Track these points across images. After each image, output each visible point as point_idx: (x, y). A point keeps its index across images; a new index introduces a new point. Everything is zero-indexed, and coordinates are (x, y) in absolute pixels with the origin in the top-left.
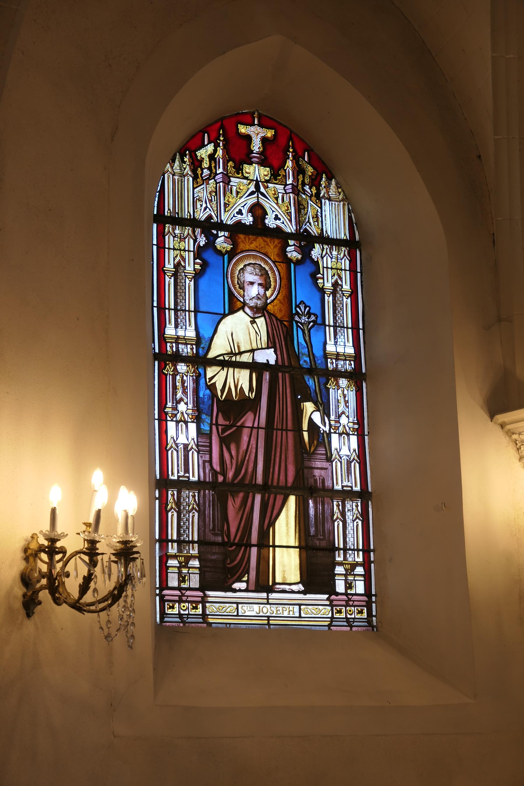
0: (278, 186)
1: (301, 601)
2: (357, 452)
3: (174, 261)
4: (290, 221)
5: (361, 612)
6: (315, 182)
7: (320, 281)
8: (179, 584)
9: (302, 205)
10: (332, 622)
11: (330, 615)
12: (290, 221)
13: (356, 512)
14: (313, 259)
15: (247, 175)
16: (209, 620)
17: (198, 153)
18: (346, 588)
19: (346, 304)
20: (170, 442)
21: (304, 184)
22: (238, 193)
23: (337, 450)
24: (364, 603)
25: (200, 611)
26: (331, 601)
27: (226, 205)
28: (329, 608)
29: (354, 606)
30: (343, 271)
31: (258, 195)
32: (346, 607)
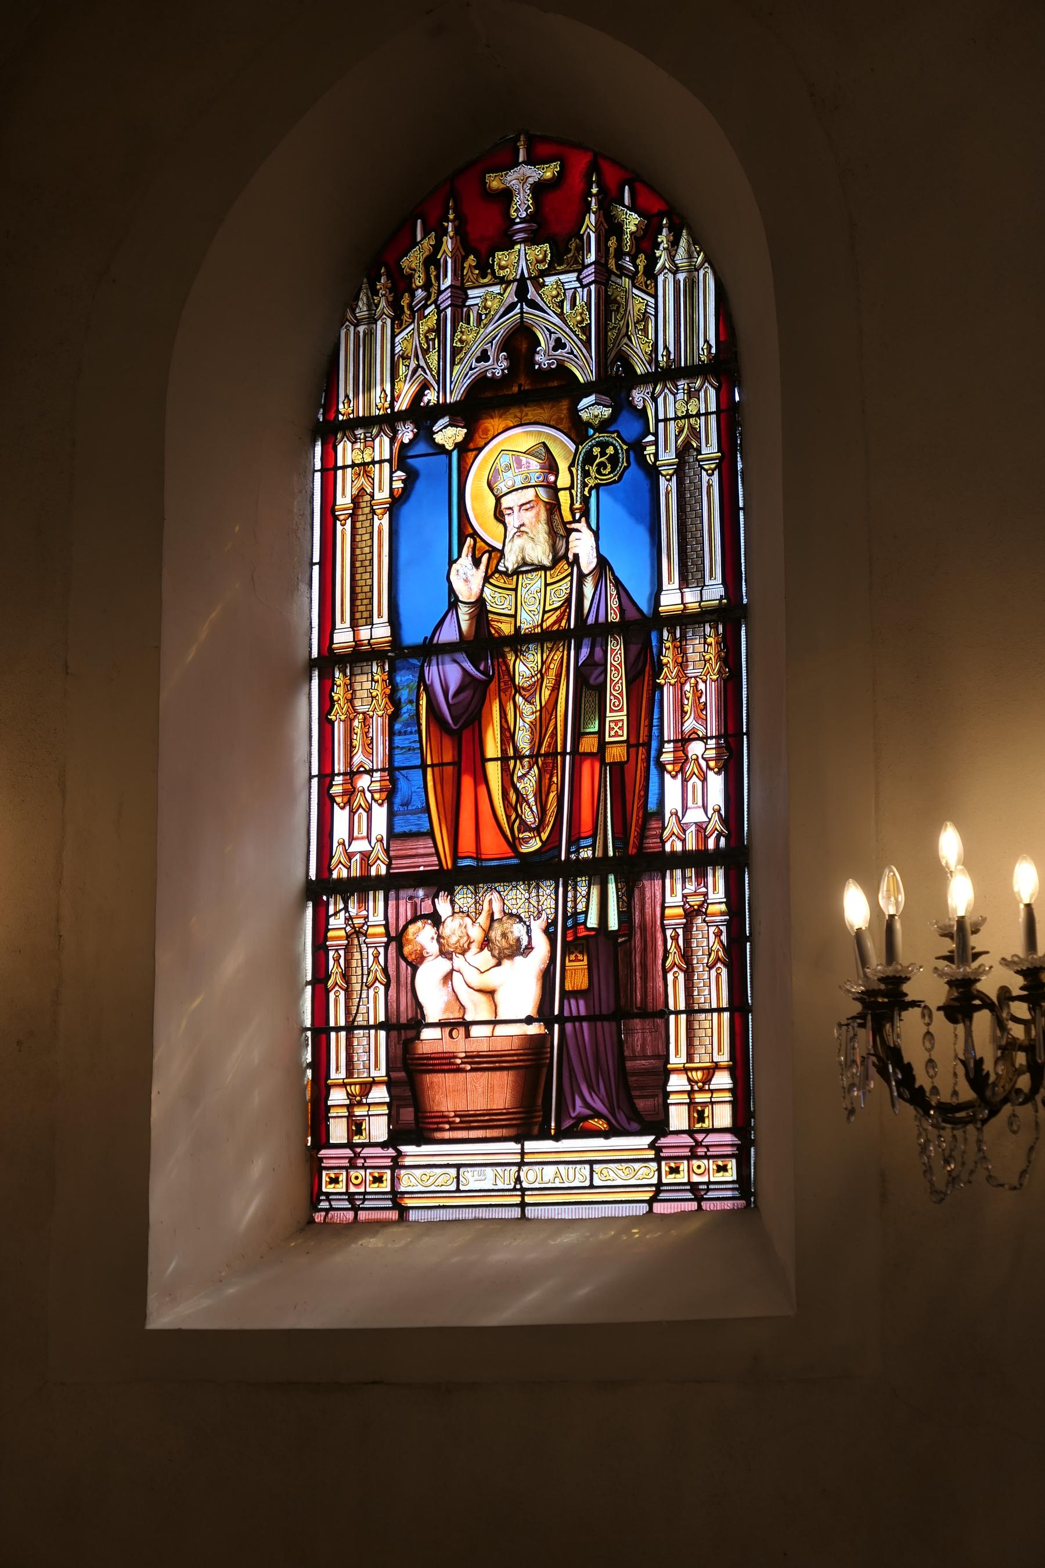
0: (563, 278)
1: (430, 1158)
2: (723, 812)
3: (676, 442)
4: (587, 344)
5: (722, 1169)
6: (646, 242)
7: (651, 449)
8: (350, 1138)
9: (616, 301)
10: (658, 1191)
11: (655, 1181)
12: (587, 344)
13: (716, 946)
14: (635, 407)
15: (502, 273)
16: (406, 1201)
17: (405, 263)
18: (350, 1134)
19: (667, 493)
20: (338, 852)
21: (619, 254)
22: (479, 319)
23: (676, 814)
24: (728, 1151)
25: (386, 1187)
26: (658, 1150)
27: (455, 352)
28: (654, 1165)
29: (365, 1168)
30: (703, 418)
31: (522, 308)
32: (688, 1158)
